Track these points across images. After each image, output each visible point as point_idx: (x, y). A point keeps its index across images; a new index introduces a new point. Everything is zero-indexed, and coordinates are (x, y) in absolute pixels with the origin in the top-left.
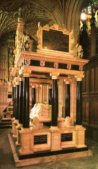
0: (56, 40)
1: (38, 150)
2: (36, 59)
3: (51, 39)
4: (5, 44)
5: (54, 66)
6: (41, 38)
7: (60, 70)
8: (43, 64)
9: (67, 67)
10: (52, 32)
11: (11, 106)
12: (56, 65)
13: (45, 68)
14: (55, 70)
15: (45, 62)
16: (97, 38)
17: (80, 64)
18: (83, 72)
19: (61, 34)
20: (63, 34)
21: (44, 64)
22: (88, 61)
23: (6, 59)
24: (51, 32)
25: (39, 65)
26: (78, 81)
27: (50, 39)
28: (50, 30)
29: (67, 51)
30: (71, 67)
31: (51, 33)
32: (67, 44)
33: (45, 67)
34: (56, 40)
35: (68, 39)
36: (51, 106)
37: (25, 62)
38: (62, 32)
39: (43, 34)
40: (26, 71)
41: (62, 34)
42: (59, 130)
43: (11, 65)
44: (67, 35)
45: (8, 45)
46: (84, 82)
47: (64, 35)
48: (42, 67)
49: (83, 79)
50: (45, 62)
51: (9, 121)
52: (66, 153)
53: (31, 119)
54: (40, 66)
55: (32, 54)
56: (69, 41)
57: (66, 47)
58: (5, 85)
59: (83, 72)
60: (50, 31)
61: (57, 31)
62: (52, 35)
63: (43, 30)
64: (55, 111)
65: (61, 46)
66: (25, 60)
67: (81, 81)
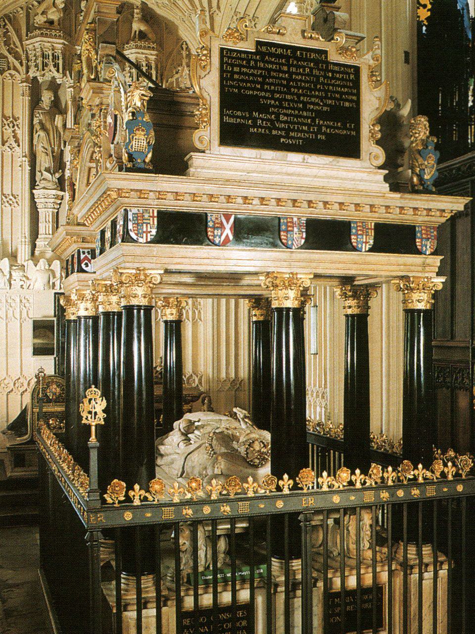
0: (288, 97)
2: (186, 206)
3: (266, 91)
4: (11, 59)
8: (222, 227)
10: (271, 55)
11: (49, 401)
15: (232, 220)
17: (420, 219)
18: (437, 260)
19: (316, 62)
20: (327, 63)
22: (467, 200)
23: (20, 136)
24: (263, 55)
27: (261, 90)
28: (259, 43)
31: (262, 60)
32: (353, 115)
36: (267, 436)
37: (130, 226)
39: (222, 71)
43: (47, 175)
45: (32, 64)
46: (441, 315)
47: (336, 68)
49: (435, 295)
50: (236, 220)
51: (289, 365)
52: (367, 326)
55: (167, 183)
56: (358, 95)
58: (17, 284)
59: (437, 260)
60: (257, 52)
61: (294, 49)
62: (269, 70)
63: (222, 50)
65: (320, 127)
66: (130, 217)
67: (428, 307)
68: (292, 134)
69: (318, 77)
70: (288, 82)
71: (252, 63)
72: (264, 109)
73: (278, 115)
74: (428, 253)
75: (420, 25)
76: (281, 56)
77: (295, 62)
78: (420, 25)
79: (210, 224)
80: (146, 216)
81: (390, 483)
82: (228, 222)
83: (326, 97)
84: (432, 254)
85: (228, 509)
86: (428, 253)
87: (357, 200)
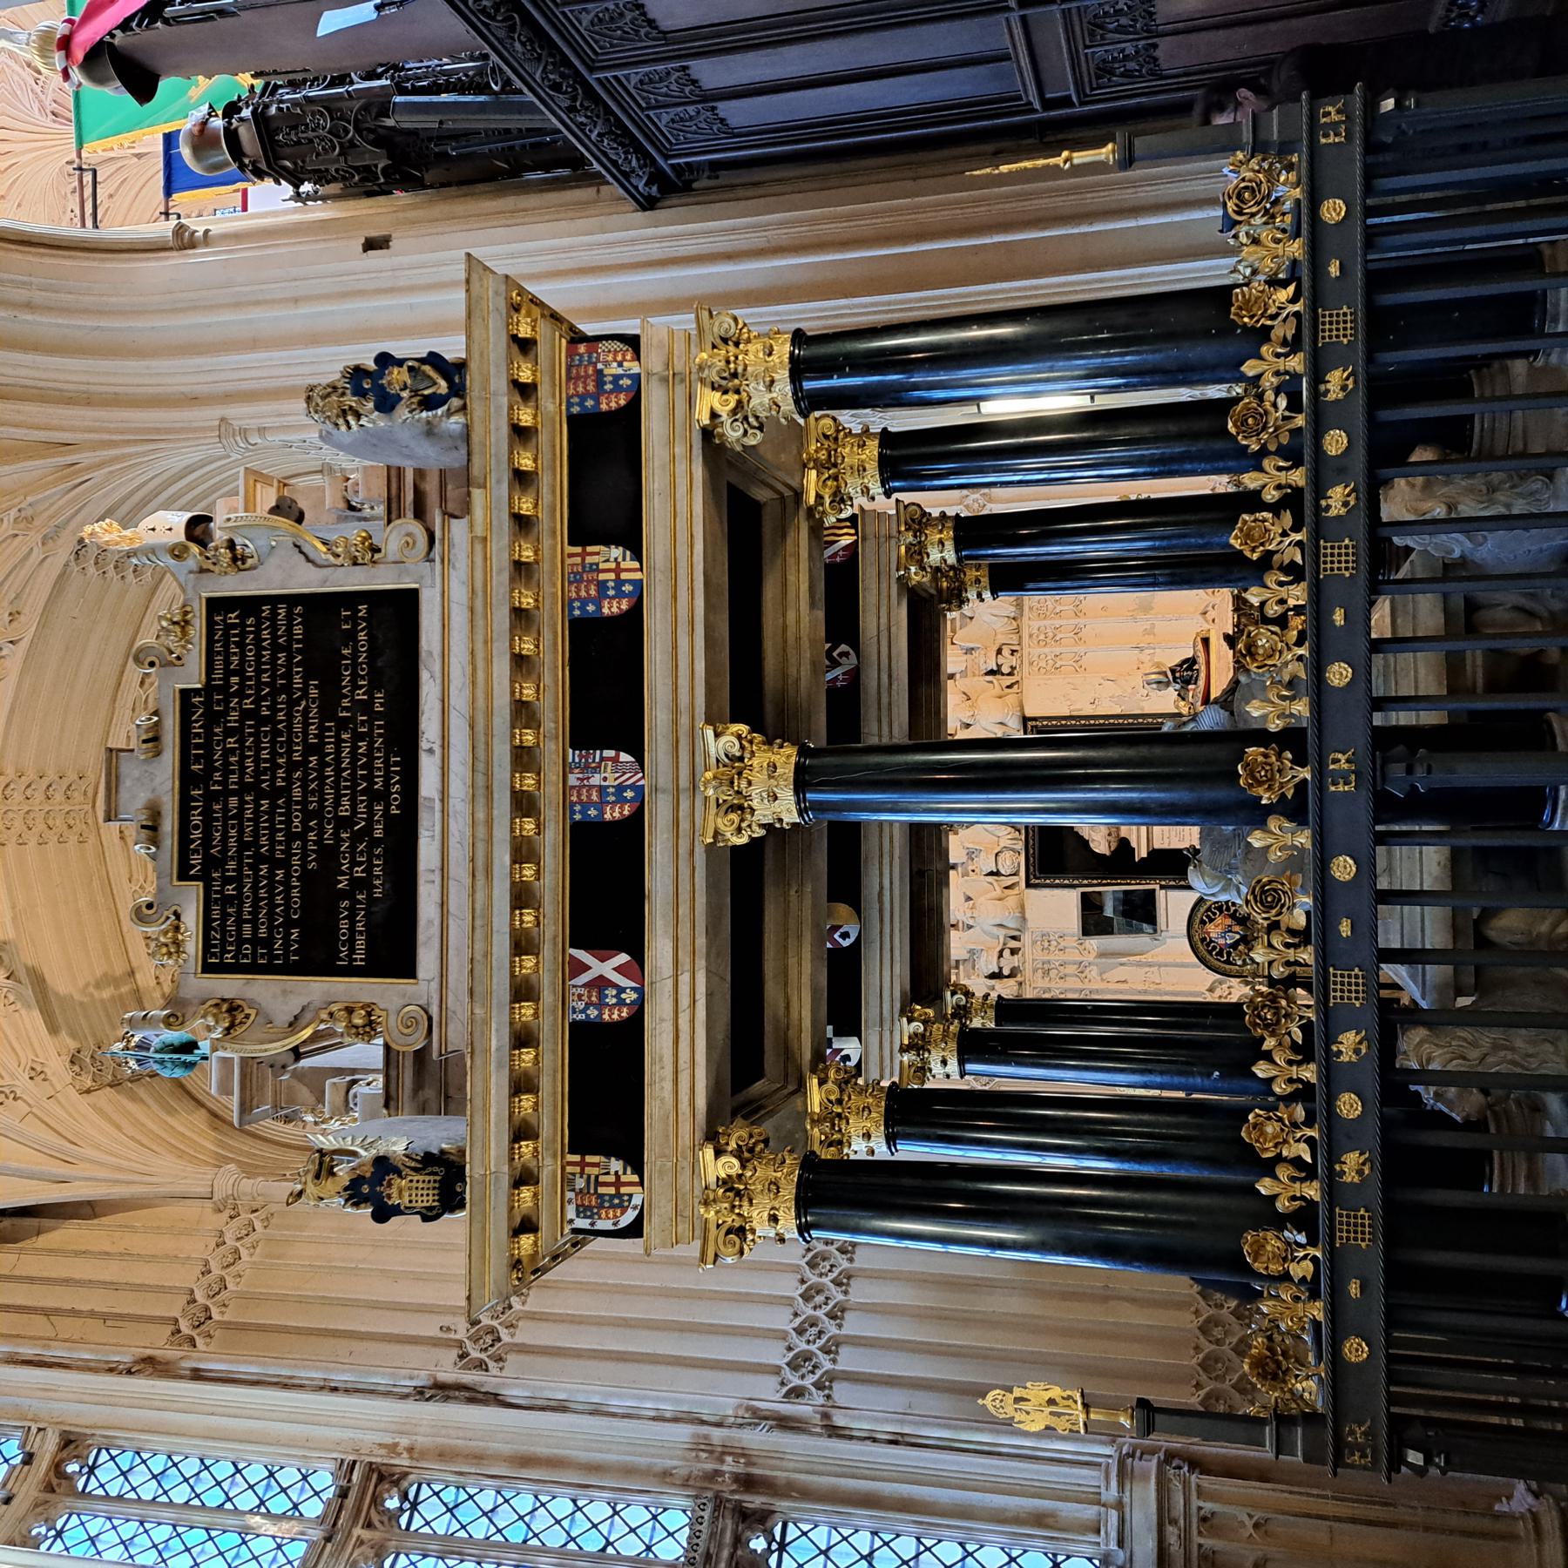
3: (288, 852)
8: (601, 983)
13: (659, 948)
15: (582, 955)
16: (1562, 1512)
19: (212, 719)
20: (209, 688)
21: (609, 967)
24: (210, 863)
25: (632, 1031)
26: (788, 406)
28: (184, 875)
31: (220, 863)
33: (638, 955)
34: (297, 793)
35: (249, 605)
38: (185, 694)
40: (820, 466)
41: (208, 704)
44: (211, 624)
48: (640, 991)
54: (636, 1020)
56: (274, 600)
57: (352, 635)
60: (205, 877)
61: (187, 779)
62: (243, 846)
63: (207, 968)
64: (1156, 795)
65: (245, 714)
69: (245, 714)
71: (230, 890)
72: (329, 855)
76: (207, 813)
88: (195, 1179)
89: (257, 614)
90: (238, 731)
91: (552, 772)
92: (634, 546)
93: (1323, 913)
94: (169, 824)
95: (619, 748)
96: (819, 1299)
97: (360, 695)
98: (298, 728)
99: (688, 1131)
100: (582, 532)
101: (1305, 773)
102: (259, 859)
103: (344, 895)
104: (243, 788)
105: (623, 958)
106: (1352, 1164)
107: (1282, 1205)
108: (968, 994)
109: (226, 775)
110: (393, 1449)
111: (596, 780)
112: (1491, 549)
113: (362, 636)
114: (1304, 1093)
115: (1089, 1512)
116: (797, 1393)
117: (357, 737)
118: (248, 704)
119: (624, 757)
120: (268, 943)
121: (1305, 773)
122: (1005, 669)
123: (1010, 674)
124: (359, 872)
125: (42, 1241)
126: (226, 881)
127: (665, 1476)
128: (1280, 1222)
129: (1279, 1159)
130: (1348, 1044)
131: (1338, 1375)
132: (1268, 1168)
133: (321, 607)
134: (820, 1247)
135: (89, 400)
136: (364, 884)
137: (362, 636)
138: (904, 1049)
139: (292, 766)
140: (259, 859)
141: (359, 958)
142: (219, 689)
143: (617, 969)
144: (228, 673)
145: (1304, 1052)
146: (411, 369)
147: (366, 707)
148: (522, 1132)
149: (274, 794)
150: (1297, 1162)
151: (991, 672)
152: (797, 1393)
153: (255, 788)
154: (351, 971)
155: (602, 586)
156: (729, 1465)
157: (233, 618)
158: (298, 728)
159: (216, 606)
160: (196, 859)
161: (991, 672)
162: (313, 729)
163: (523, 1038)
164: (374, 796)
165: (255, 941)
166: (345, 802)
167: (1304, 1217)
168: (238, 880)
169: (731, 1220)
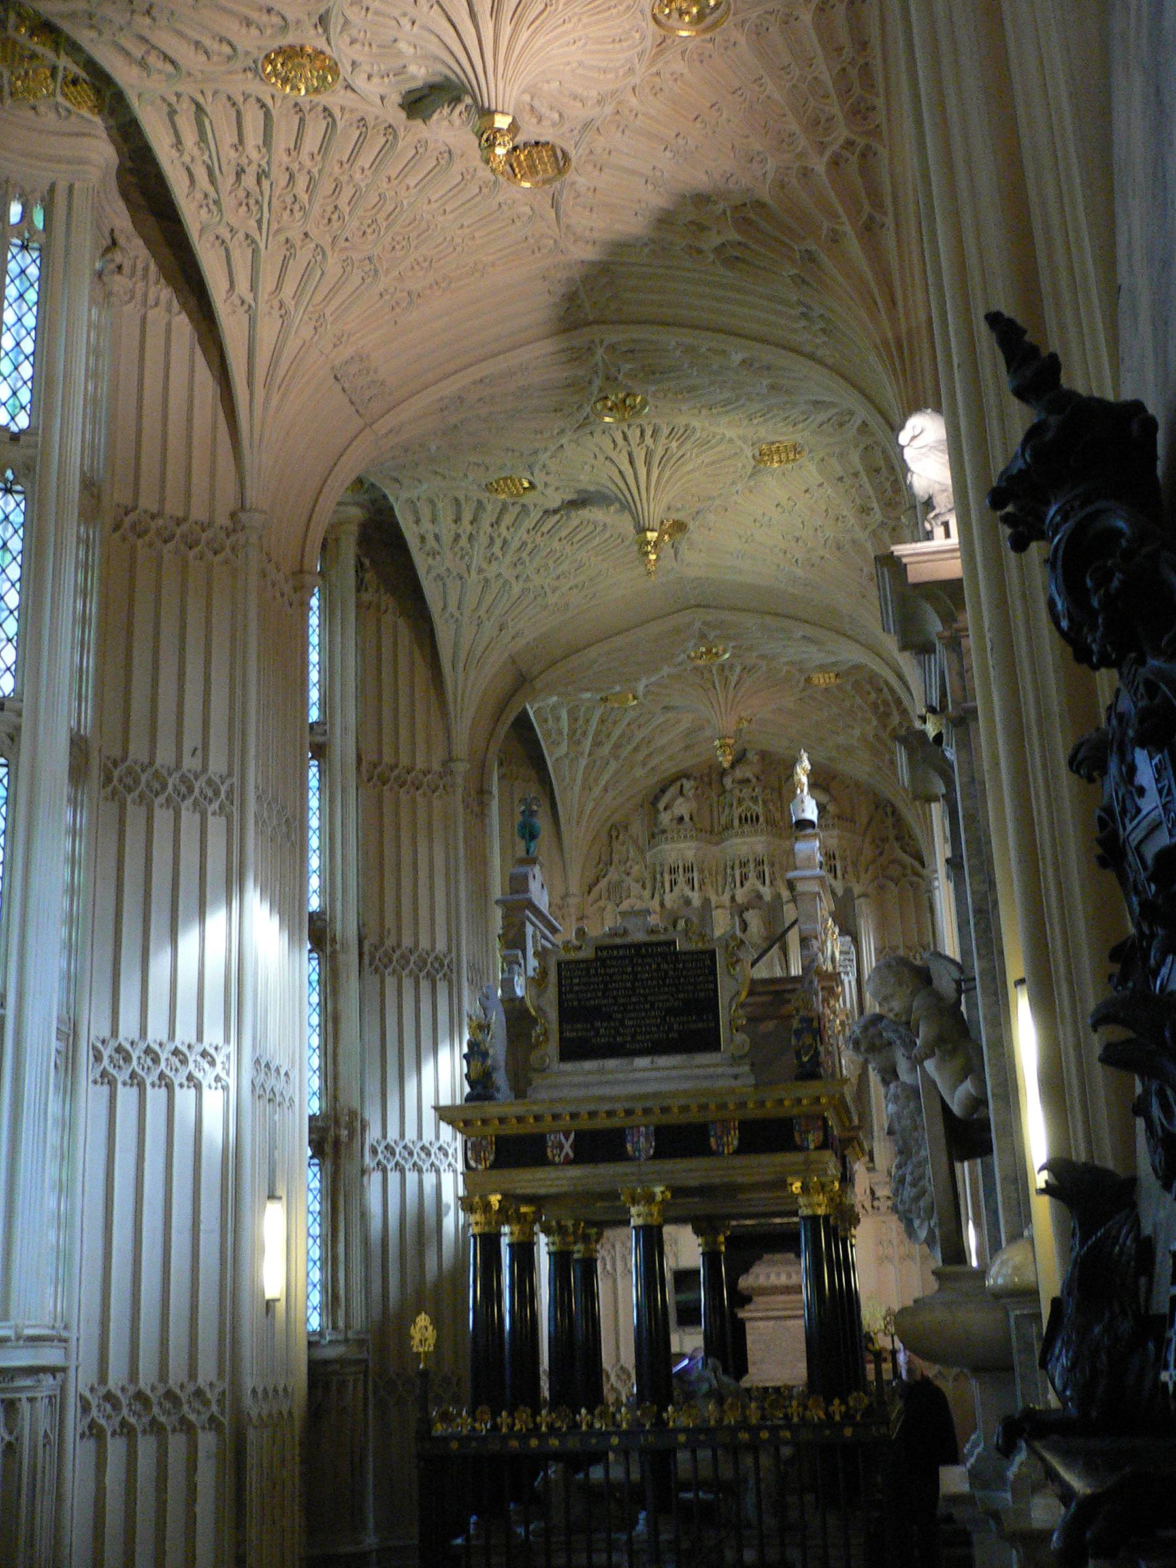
1: (945, 838)
5: (629, 1147)
6: (547, 1008)
7: (668, 1165)
8: (561, 1147)
9: (712, 1140)
10: (612, 958)
12: (641, 1143)
13: (575, 1172)
14: (634, 1170)
15: (572, 1136)
19: (663, 956)
20: (676, 954)
24: (603, 961)
25: (541, 1160)
28: (599, 949)
29: (710, 1042)
30: (740, 1139)
31: (604, 966)
34: (634, 999)
42: (823, 655)
48: (559, 1164)
51: (978, 1191)
53: (884, 1205)
54: (551, 1163)
60: (597, 959)
61: (638, 946)
63: (559, 964)
68: (639, 1038)
69: (666, 972)
70: (633, 984)
71: (592, 971)
72: (609, 1017)
73: (622, 1022)
74: (812, 1146)
75: (72, 729)
76: (624, 957)
77: (640, 961)
78: (72, 729)
79: (550, 1144)
80: (484, 1143)
81: (754, 1421)
82: (567, 1139)
83: (679, 992)
84: (817, 1148)
85: (557, 1443)
86: (812, 1146)
87: (592, 1107)
88: (461, 747)
89: (710, 974)
90: (658, 969)
91: (644, 1120)
92: (739, 1151)
93: (600, 1434)
94: (618, 941)
95: (656, 1148)
96: (423, 1155)
97: (675, 1027)
98: (661, 998)
99: (506, 1186)
100: (746, 1127)
101: (647, 1427)
102: (606, 984)
103: (592, 1025)
104: (635, 973)
105: (572, 1155)
106: (514, 1443)
107: (499, 1420)
108: (597, 1241)
109: (641, 965)
110: (334, 940)
111: (642, 1139)
112: (750, 1498)
113: (700, 1025)
114: (537, 1427)
115: (341, 1324)
116: (374, 1151)
117: (658, 1026)
118: (671, 973)
119: (652, 1152)
120: (571, 991)
121: (647, 1427)
122: (876, 1203)
123: (873, 1207)
124: (602, 1031)
125: (417, 654)
126: (596, 969)
127: (335, 1098)
128: (494, 1419)
129: (514, 1419)
130: (554, 1442)
131: (445, 1440)
132: (511, 1414)
133: (710, 1006)
134: (451, 1151)
135: (1114, 339)
136: (597, 1034)
137: (700, 1025)
138: (558, 1223)
139: (645, 997)
140: (606, 984)
141: (568, 1034)
142: (677, 957)
143: (567, 1154)
144: (684, 962)
145: (551, 1427)
146: (811, 1045)
147: (671, 1029)
148: (502, 1120)
149: (634, 989)
150: (514, 1425)
151: (872, 1192)
152: (374, 1151)
153: (636, 979)
154: (561, 1032)
155: (721, 1138)
156: (344, 1133)
157: (708, 962)
158: (661, 998)
159: (712, 953)
160: (605, 953)
161: (872, 1192)
162: (660, 1005)
163: (537, 1118)
164: (634, 1036)
165: (571, 985)
166: (630, 1023)
167: (496, 1428)
168: (596, 974)
169: (475, 1206)
